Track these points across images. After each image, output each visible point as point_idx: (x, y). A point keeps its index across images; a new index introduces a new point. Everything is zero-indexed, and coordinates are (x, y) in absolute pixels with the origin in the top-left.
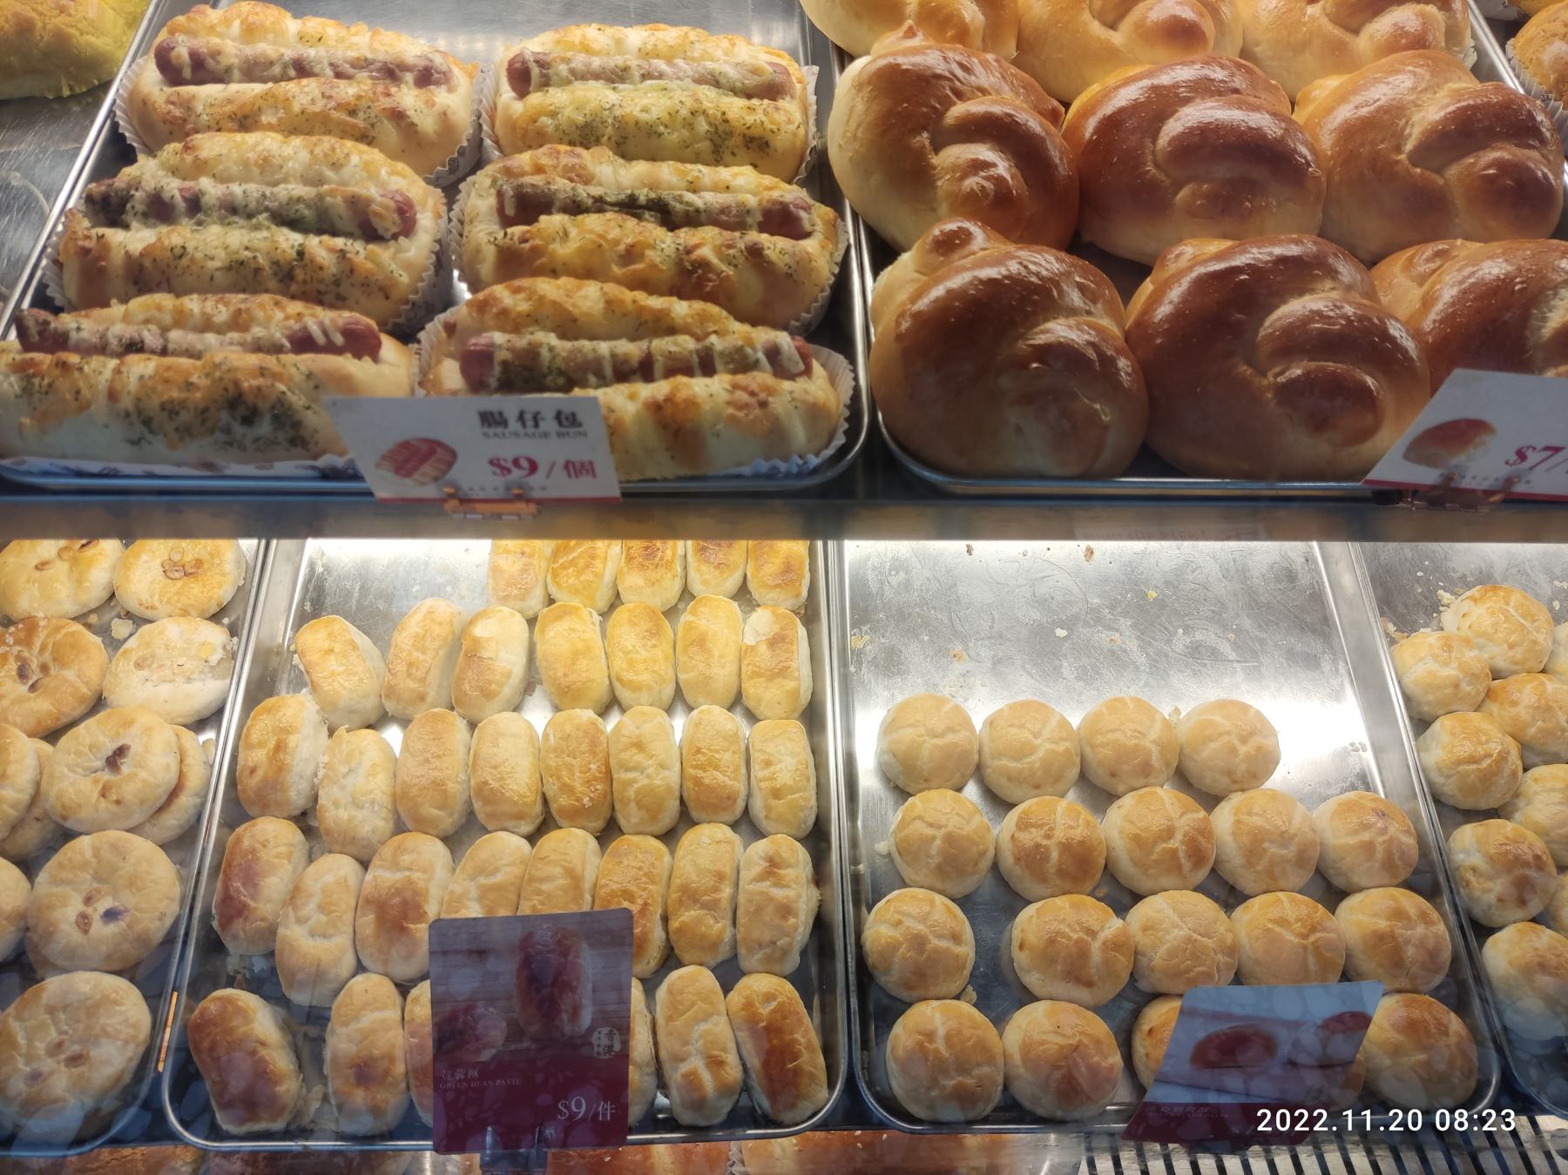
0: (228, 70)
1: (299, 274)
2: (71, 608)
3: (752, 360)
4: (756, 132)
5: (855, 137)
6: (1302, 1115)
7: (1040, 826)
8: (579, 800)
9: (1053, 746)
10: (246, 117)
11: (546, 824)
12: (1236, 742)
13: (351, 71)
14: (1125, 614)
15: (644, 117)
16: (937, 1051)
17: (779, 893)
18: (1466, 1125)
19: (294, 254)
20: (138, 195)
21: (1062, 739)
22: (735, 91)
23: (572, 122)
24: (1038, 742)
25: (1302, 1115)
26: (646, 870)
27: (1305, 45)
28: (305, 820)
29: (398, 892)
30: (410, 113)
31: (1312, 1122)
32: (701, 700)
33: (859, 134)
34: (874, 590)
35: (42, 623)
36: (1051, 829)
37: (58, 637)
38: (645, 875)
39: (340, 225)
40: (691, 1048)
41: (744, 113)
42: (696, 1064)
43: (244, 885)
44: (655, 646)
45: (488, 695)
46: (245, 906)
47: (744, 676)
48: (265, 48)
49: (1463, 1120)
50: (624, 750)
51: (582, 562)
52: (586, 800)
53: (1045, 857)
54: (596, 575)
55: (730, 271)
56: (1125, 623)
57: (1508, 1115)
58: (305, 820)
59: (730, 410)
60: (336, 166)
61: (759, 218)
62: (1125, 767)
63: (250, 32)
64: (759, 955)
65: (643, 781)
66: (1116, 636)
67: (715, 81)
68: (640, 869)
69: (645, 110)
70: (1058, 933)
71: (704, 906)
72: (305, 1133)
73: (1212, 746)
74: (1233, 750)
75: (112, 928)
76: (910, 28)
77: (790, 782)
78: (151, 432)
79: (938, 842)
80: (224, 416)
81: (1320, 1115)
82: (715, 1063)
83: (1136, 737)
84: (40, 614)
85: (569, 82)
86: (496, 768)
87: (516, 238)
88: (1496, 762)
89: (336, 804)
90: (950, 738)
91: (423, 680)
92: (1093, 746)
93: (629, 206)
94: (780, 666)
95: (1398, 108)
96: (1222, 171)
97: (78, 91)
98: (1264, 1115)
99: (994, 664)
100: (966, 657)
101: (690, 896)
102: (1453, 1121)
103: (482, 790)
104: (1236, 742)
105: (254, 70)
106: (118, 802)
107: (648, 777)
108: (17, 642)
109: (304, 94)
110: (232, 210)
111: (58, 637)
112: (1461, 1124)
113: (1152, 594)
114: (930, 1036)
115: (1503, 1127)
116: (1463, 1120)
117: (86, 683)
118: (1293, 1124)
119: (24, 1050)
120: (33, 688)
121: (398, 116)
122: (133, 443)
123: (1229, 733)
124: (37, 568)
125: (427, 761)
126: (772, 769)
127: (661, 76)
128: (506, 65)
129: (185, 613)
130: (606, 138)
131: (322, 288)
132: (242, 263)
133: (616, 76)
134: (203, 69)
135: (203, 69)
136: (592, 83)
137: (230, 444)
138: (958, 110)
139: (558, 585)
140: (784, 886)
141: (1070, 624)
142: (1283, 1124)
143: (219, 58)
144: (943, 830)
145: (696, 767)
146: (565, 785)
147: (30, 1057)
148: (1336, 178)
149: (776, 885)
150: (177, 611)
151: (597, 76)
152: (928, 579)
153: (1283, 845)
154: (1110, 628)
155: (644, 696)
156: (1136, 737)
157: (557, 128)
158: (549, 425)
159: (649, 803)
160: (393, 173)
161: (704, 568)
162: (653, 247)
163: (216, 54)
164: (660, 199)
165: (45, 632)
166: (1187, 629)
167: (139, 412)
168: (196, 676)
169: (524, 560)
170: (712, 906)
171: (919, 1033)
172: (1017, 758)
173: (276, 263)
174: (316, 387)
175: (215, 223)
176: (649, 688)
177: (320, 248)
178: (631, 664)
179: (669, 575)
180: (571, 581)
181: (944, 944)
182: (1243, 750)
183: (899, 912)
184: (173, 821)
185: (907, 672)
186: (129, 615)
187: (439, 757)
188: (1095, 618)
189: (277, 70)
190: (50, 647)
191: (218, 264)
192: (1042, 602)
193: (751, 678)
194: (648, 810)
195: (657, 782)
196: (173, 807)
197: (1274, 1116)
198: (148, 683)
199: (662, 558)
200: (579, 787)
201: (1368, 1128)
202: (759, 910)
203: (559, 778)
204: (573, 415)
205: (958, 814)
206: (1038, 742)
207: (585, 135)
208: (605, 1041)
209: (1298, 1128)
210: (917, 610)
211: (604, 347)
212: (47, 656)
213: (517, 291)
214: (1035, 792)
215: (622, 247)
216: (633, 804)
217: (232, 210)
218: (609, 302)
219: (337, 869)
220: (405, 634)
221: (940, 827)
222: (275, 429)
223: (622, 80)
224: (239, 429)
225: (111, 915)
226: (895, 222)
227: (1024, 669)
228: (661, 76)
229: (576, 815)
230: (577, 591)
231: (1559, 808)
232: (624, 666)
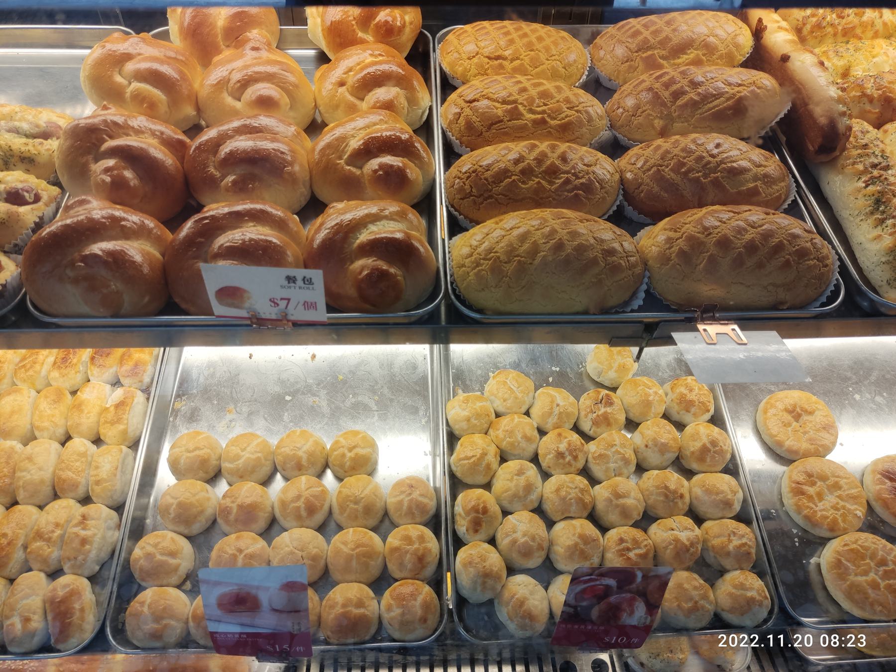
4: (28, 155)
6: (744, 638)
12: (346, 451)
14: (324, 388)
17: (83, 533)
21: (256, 452)
24: (243, 454)
27: (337, 107)
34: (194, 378)
36: (236, 498)
40: (16, 613)
44: (55, 408)
49: (836, 640)
51: (29, 366)
54: (35, 372)
56: (323, 393)
57: (862, 638)
62: (288, 466)
67: (17, 131)
71: (44, 540)
73: (336, 453)
74: (343, 455)
79: (174, 506)
82: (26, 620)
83: (295, 450)
88: (479, 459)
90: (197, 452)
95: (343, 138)
96: (241, 170)
98: (723, 638)
100: (234, 411)
101: (39, 535)
102: (830, 641)
104: (346, 451)
107: (31, 475)
112: (835, 643)
113: (341, 377)
115: (859, 644)
116: (834, 640)
118: (739, 643)
123: (343, 447)
139: (16, 379)
141: (293, 394)
142: (733, 643)
148: (314, 172)
152: (225, 372)
153: (356, 503)
154: (314, 395)
155: (45, 434)
156: (295, 450)
158: (300, 283)
166: (355, 395)
170: (49, 540)
179: (73, 372)
181: (164, 558)
182: (349, 455)
185: (200, 420)
188: (309, 390)
192: (281, 382)
193: (104, 424)
195: (35, 477)
197: (728, 638)
201: (782, 645)
204: (311, 279)
209: (742, 645)
210: (215, 388)
227: (264, 417)
230: (25, 380)
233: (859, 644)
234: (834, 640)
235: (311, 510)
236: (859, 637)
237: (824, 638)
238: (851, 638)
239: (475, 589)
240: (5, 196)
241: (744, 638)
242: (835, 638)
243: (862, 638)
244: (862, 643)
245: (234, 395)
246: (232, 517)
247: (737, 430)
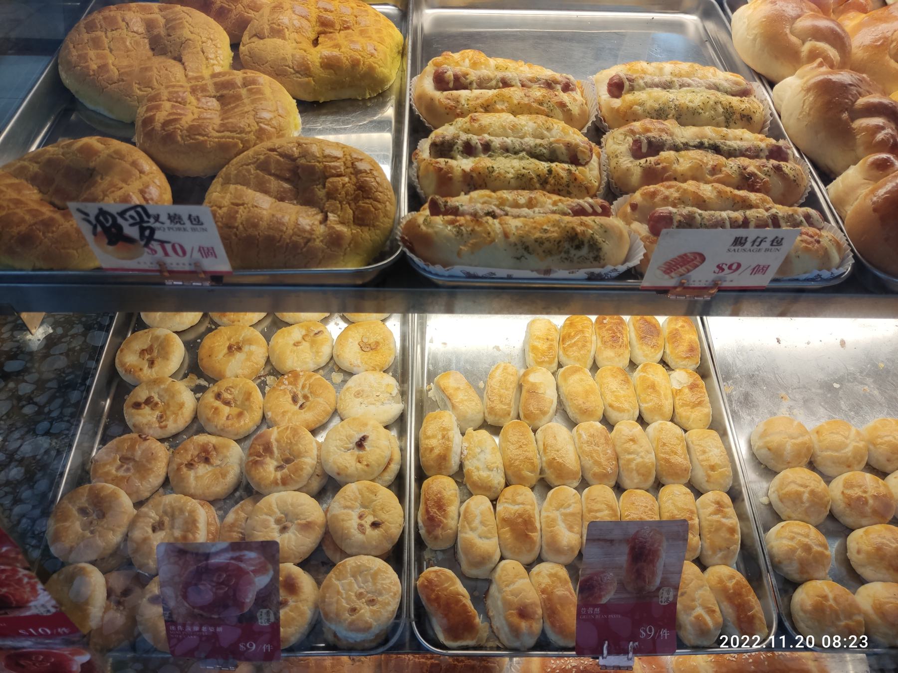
0: (471, 83)
1: (552, 181)
2: (312, 366)
3: (799, 220)
4: (745, 113)
5: (809, 114)
6: (745, 639)
7: (860, 486)
8: (604, 469)
9: (857, 444)
10: (488, 106)
11: (584, 484)
13: (529, 84)
14: (868, 375)
15: (691, 105)
16: (831, 606)
19: (547, 172)
20: (459, 142)
22: (727, 92)
23: (652, 108)
26: (649, 507)
28: (460, 475)
29: (520, 516)
30: (568, 104)
31: (750, 644)
32: (656, 418)
33: (812, 113)
34: (731, 362)
35: (301, 374)
37: (312, 381)
38: (650, 510)
39: (561, 157)
40: (697, 603)
41: (739, 103)
42: (699, 611)
43: (438, 510)
45: (544, 413)
46: (441, 522)
47: (677, 406)
48: (484, 72)
49: (838, 641)
50: (624, 443)
51: (580, 344)
52: (609, 469)
53: (866, 502)
55: (767, 179)
56: (869, 380)
57: (864, 639)
58: (460, 475)
59: (804, 245)
60: (548, 129)
61: (767, 153)
63: (474, 65)
64: (720, 555)
65: (639, 460)
66: (866, 387)
68: (646, 507)
69: (691, 101)
70: (883, 544)
75: (376, 533)
76: (821, 62)
77: (719, 462)
78: (529, 253)
80: (566, 245)
82: (711, 612)
84: (298, 369)
85: (644, 89)
86: (558, 451)
87: (652, 163)
89: (478, 469)
91: (509, 404)
92: (875, 445)
93: (700, 146)
94: (699, 400)
97: (373, 96)
98: (724, 639)
99: (804, 402)
102: (832, 641)
103: (551, 463)
105: (482, 84)
106: (367, 465)
107: (642, 457)
108: (290, 383)
109: (516, 94)
110: (506, 150)
111: (312, 381)
112: (837, 644)
114: (825, 597)
115: (861, 645)
116: (836, 641)
117: (329, 405)
119: (344, 596)
120: (301, 407)
121: (562, 105)
122: (518, 259)
124: (294, 345)
125: (521, 447)
126: (706, 455)
127: (689, 85)
128: (607, 81)
129: (374, 369)
130: (671, 115)
131: (560, 188)
132: (523, 175)
133: (667, 86)
134: (460, 83)
135: (460, 83)
136: (655, 89)
137: (566, 259)
138: (861, 101)
140: (728, 518)
143: (467, 77)
144: (809, 489)
145: (665, 453)
146: (596, 461)
147: (348, 599)
149: (724, 517)
150: (371, 368)
151: (657, 86)
154: (862, 383)
157: (644, 111)
159: (642, 472)
160: (574, 133)
161: (645, 347)
162: (726, 166)
163: (465, 75)
164: (715, 144)
165: (304, 378)
167: (523, 243)
168: (386, 402)
169: (549, 343)
171: (818, 596)
172: (837, 451)
173: (539, 176)
174: (606, 232)
175: (499, 156)
176: (628, 411)
177: (560, 168)
178: (617, 397)
180: (576, 354)
183: (792, 532)
184: (390, 475)
186: (340, 370)
187: (526, 445)
189: (494, 83)
190: (308, 386)
191: (511, 175)
193: (682, 406)
194: (643, 475)
196: (388, 470)
197: (805, 639)
198: (363, 405)
199: (622, 342)
200: (604, 463)
202: (717, 530)
203: (592, 457)
205: (814, 480)
206: (848, 441)
207: (660, 114)
211: (724, 214)
212: (306, 391)
213: (669, 187)
214: (848, 469)
215: (709, 166)
216: (634, 472)
217: (506, 150)
218: (719, 192)
219: (480, 504)
220: (494, 380)
221: (807, 487)
222: (589, 252)
223: (670, 87)
224: (573, 252)
225: (375, 525)
226: (832, 156)
227: (821, 405)
228: (689, 85)
229: (602, 478)
230: (579, 360)
232: (613, 399)
233: (861, 645)
234: (836, 641)
236: (861, 638)
237: (826, 639)
238: (853, 639)
239: (504, 582)
240: (767, 154)
241: (745, 639)
242: (837, 639)
243: (864, 639)
244: (864, 644)
245: (780, 380)
246: (868, 509)
247: (739, 436)
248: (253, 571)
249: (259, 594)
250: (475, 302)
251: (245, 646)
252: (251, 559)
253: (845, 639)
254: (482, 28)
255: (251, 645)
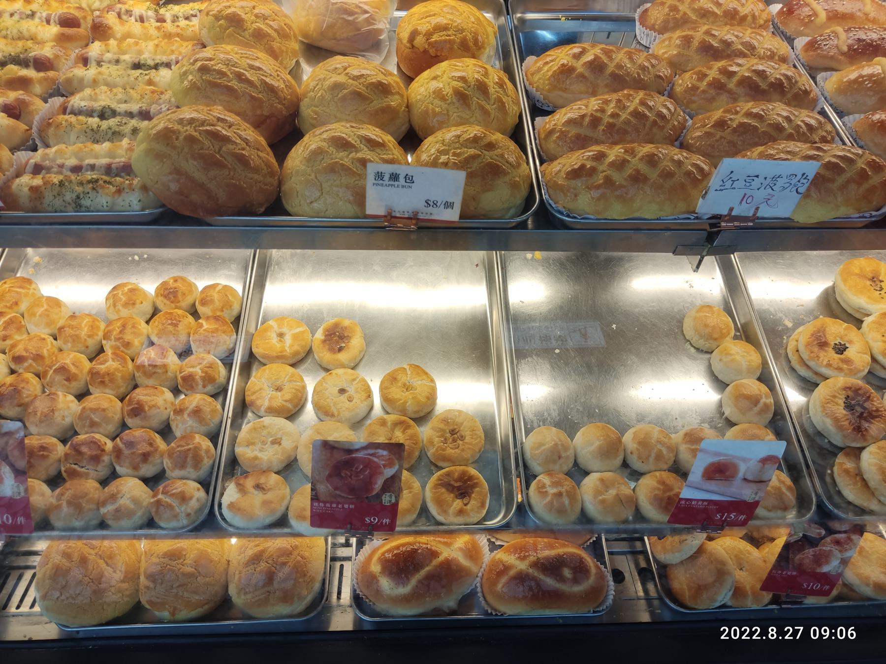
6: (746, 630)
18: (775, 636)
25: (746, 630)
31: (751, 634)
49: (774, 633)
72: (232, 352)
81: (756, 630)
98: (725, 630)
112: (772, 635)
116: (774, 633)
142: (735, 635)
208: (388, 499)
209: (743, 637)
231: (263, 164)
235: (168, 144)
237: (815, 630)
242: (772, 630)
248: (385, 466)
249: (387, 481)
250: (156, 270)
251: (370, 520)
252: (383, 456)
253: (764, 638)
254: (116, 229)
255: (374, 519)
